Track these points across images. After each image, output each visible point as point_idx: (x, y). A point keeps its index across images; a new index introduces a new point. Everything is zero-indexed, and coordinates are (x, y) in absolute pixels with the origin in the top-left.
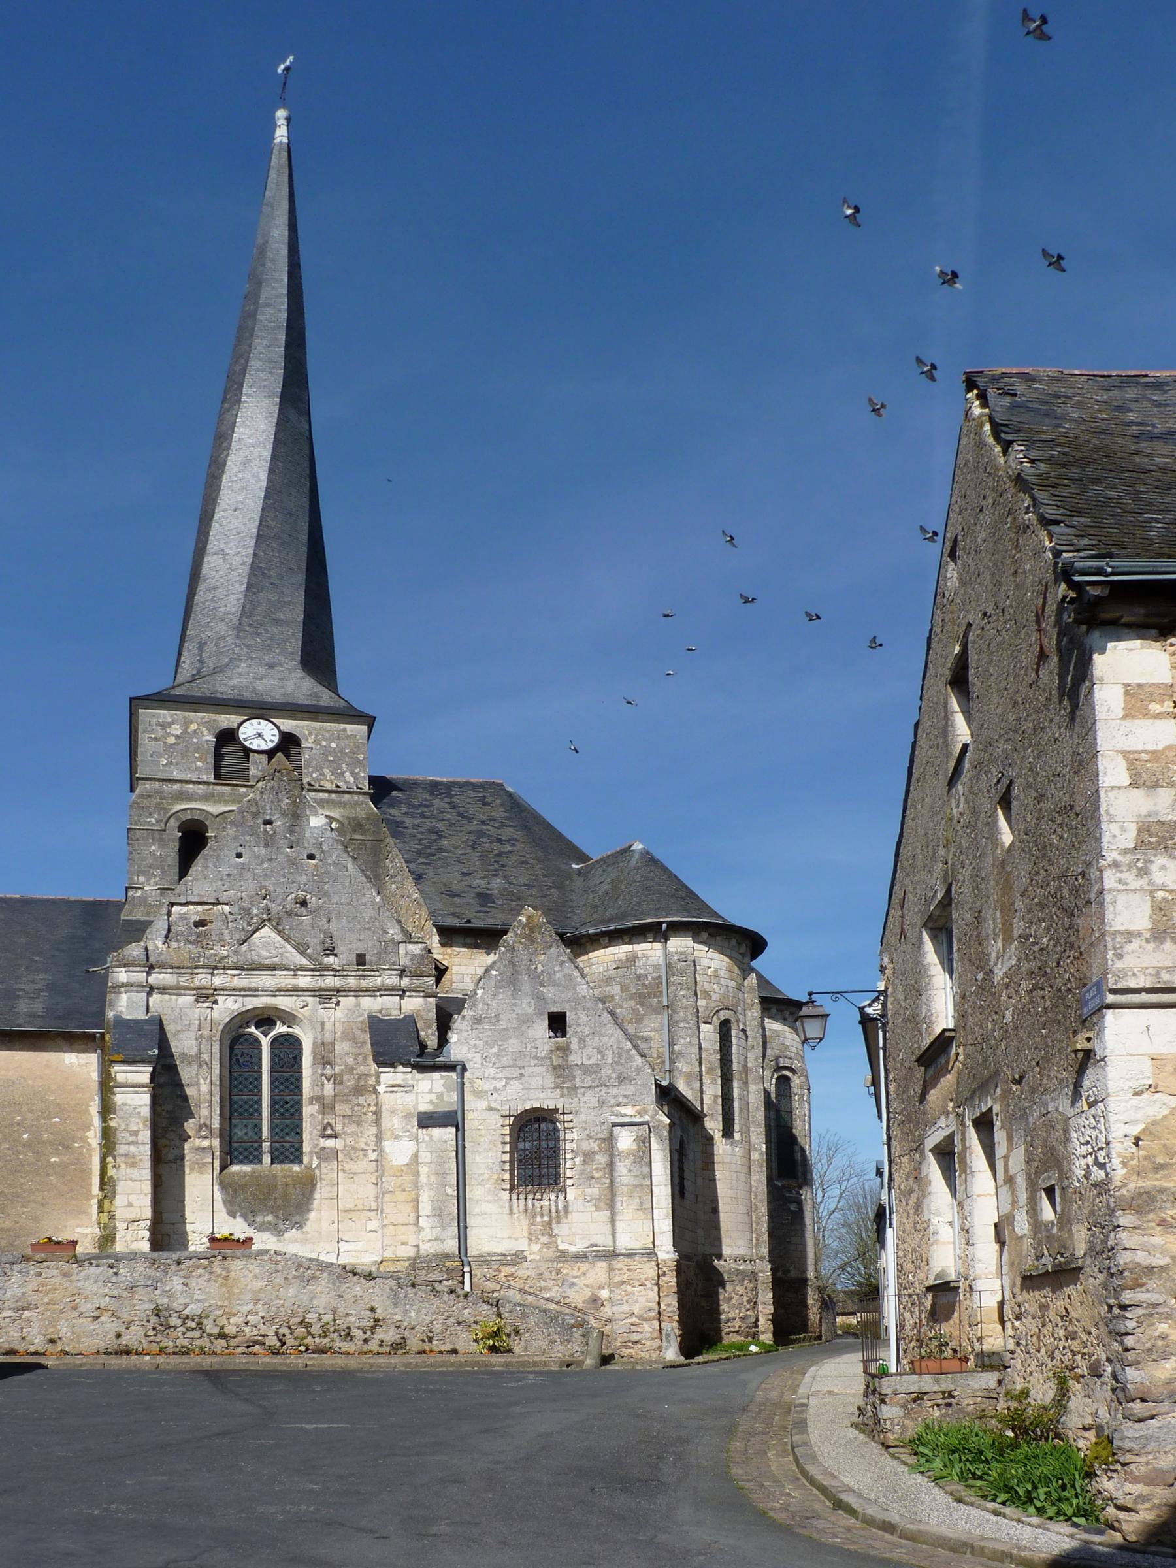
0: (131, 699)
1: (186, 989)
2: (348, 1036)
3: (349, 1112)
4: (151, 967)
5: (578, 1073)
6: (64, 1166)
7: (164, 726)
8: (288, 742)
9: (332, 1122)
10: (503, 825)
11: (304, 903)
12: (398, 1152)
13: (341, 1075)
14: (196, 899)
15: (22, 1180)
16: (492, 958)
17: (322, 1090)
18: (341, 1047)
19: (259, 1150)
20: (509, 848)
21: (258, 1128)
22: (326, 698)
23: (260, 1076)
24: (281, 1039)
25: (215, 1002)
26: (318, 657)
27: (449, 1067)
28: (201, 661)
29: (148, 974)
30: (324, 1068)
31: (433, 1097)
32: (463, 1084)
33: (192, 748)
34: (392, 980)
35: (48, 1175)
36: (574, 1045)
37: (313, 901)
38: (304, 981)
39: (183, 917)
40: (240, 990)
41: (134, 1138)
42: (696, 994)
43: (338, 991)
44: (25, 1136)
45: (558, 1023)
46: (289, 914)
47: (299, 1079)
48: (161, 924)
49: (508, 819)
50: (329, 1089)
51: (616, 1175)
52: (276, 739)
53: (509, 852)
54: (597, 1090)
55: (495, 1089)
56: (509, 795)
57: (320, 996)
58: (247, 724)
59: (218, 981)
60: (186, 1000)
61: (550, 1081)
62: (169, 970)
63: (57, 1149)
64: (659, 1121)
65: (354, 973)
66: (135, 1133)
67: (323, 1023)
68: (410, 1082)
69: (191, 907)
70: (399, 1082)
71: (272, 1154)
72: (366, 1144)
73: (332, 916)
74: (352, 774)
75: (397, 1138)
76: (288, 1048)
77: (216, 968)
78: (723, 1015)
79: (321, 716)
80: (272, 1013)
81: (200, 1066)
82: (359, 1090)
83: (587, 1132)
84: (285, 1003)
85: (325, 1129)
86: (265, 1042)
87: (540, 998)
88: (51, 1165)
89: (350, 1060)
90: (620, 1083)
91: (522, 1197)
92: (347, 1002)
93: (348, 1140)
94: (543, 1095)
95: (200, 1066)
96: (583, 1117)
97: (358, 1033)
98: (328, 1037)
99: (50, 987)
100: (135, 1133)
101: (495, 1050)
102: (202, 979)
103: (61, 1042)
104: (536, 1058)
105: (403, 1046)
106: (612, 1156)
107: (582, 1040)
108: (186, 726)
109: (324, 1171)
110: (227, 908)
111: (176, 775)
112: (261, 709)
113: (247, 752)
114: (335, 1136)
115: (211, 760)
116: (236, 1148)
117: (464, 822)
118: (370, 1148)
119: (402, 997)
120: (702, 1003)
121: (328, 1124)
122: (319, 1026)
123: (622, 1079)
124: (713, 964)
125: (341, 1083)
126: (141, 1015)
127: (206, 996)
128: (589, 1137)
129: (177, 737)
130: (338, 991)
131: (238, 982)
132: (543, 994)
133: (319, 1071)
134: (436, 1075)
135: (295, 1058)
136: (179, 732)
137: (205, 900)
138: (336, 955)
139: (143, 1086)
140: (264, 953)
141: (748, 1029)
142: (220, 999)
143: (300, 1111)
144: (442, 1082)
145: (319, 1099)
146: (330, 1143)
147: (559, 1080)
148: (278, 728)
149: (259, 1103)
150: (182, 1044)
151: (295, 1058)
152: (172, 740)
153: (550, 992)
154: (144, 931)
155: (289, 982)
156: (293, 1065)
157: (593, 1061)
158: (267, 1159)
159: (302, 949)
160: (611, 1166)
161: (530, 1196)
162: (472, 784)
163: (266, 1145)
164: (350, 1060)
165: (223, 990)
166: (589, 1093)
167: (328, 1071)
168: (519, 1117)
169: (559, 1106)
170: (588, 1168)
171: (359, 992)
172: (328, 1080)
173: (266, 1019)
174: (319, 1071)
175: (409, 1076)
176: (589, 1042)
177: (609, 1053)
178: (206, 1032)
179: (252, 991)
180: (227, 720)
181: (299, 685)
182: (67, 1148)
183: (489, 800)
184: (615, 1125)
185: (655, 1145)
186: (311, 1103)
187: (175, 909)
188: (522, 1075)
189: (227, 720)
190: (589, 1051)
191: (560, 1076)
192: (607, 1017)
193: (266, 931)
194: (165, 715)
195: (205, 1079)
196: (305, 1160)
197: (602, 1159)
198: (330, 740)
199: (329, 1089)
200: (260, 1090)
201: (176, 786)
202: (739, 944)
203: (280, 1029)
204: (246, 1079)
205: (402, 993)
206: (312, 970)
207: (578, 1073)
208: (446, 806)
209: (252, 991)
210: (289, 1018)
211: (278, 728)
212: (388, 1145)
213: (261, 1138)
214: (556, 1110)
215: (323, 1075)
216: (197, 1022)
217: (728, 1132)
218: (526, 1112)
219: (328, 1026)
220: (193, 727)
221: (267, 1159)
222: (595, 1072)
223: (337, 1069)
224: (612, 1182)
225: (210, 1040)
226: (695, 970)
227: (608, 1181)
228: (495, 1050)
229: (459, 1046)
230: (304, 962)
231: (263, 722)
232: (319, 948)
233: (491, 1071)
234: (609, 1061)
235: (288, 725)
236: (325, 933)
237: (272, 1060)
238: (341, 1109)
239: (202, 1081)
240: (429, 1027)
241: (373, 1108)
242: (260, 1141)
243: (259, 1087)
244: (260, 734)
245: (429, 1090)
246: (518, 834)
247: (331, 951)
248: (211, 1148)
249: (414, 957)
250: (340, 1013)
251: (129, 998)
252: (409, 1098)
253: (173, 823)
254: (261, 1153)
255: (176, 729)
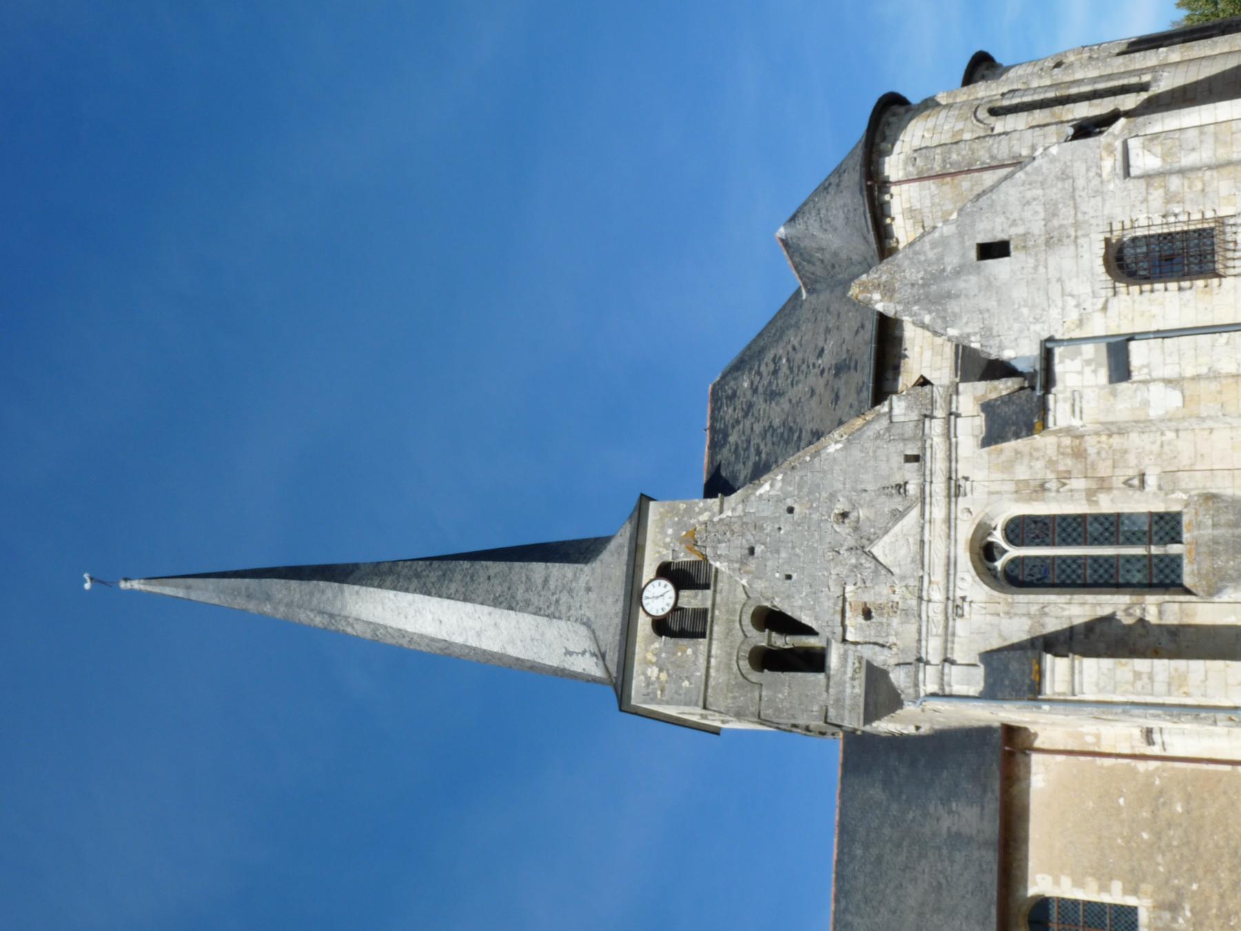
0: (642, 495)
1: (946, 627)
2: (1008, 466)
3: (1110, 463)
4: (919, 660)
5: (1056, 223)
6: (1188, 798)
7: (649, 683)
8: (665, 571)
9: (1122, 479)
10: (759, 373)
11: (844, 515)
12: (1163, 401)
13: (1058, 472)
14: (838, 618)
15: (1211, 846)
16: (906, 319)
17: (1077, 490)
18: (1022, 472)
19: (1161, 558)
20: (784, 361)
21: (1128, 559)
22: (622, 540)
23: (1060, 557)
24: (1012, 537)
25: (963, 599)
26: (579, 551)
27: (1047, 356)
28: (583, 653)
29: (927, 663)
30: (1049, 490)
31: (1088, 370)
32: (1071, 340)
33: (673, 659)
34: (936, 428)
35: (1202, 816)
36: (1020, 230)
37: (839, 508)
38: (938, 511)
39: (860, 629)
40: (948, 574)
41: (1145, 677)
42: (957, 143)
43: (950, 478)
44: (1145, 836)
45: (993, 250)
46: (856, 529)
47: (1064, 518)
48: (868, 652)
49: (751, 369)
50: (1078, 484)
51: (1198, 164)
52: (664, 582)
53: (788, 360)
54: (1079, 200)
55: (1077, 306)
56: (723, 377)
57: (957, 496)
58: (648, 608)
59: (937, 595)
60: (960, 626)
61: (1068, 251)
62: (924, 643)
63: (1164, 804)
64: (1123, 130)
65: (928, 464)
66: (1137, 675)
67: (990, 493)
68: (1068, 394)
69: (847, 622)
70: (1068, 407)
71: (1166, 544)
72: (1153, 443)
73: (860, 487)
74: (700, 513)
75: (1146, 403)
76: (1019, 530)
77: (920, 598)
78: (983, 114)
79: (640, 542)
80: (977, 545)
81: (1046, 614)
82: (1079, 454)
83: (1137, 203)
84: (965, 531)
85: (1131, 486)
86: (1014, 552)
87: (958, 272)
88: (1188, 812)
89: (1039, 465)
90: (1068, 177)
91: (1230, 263)
92: (963, 469)
93: (1146, 461)
94: (1086, 256)
95: (1046, 614)
96: (1118, 210)
97: (1003, 458)
98: (1010, 487)
99: (945, 801)
100: (1137, 675)
101: (1025, 311)
102: (935, 611)
103: (1015, 790)
104: (1036, 268)
105: (1020, 398)
106: (1171, 173)
107: (1014, 223)
108: (649, 664)
109: (1192, 485)
110: (849, 588)
111: (700, 673)
112: (634, 596)
113: (675, 608)
114: (1142, 477)
115: (683, 642)
116: (1165, 578)
117: (755, 410)
118: (1159, 439)
119: (958, 416)
120: (967, 136)
121: (1126, 483)
122: (993, 497)
123: (1064, 176)
124: (919, 134)
125: (1069, 472)
126: (980, 671)
127: (955, 608)
128: (1145, 200)
129: (661, 670)
130: (950, 478)
131: (939, 576)
132: (954, 269)
133: (1053, 494)
134: (1058, 368)
135: (1035, 522)
136: (656, 670)
137: (839, 608)
138: (906, 483)
139: (1073, 668)
140: (903, 552)
141: (1000, 92)
142: (959, 593)
143: (1106, 517)
144: (1067, 361)
145: (1090, 495)
146: (1151, 481)
147: (1066, 241)
148: (651, 581)
149: (1095, 559)
150: (1017, 630)
151: (1035, 522)
152: (663, 676)
153: (952, 261)
154: (877, 669)
155: (939, 528)
156: (1045, 524)
157: (1040, 209)
158: (1174, 549)
159: (897, 516)
160: (1182, 172)
161: (1230, 254)
162: (713, 411)
163: (1155, 550)
164: (1039, 465)
165: (948, 590)
166: (1083, 207)
167: (1053, 485)
168: (1116, 279)
169: (1102, 237)
170: (1189, 196)
171: (951, 458)
172: (1064, 484)
173: (985, 552)
174: (1053, 494)
175: (1060, 396)
176: (1016, 215)
177: (1029, 195)
178: (1001, 608)
179: (950, 564)
180: (644, 626)
181: (612, 562)
182: (1161, 792)
183: (730, 392)
184: (1127, 174)
185: (1157, 128)
186: (1096, 503)
187: (849, 637)
188: (1059, 280)
189: (644, 626)
190: (1028, 214)
191: (1060, 240)
192: (984, 201)
193: (877, 550)
194: (637, 683)
195: (1063, 609)
196: (1175, 508)
197: (1175, 183)
198: (666, 535)
199: (1078, 484)
200: (1079, 557)
201: (713, 672)
202: (894, 115)
203: (998, 537)
204: (1064, 571)
205: (952, 415)
206: (923, 503)
207: (1056, 223)
208: (737, 428)
209: (950, 564)
210: (983, 529)
211: (651, 581)
212: (1154, 413)
213: (1144, 556)
214: (1107, 241)
215: (1058, 491)
216: (989, 618)
217: (1143, 87)
218: (1109, 271)
219: (995, 487)
220: (650, 657)
221: (1174, 549)
222: (1056, 204)
223: (1051, 476)
224: (1210, 168)
225: (1011, 604)
226: (926, 148)
227: (1208, 173)
228: (1025, 311)
229: (1020, 350)
230: (915, 513)
231: (646, 594)
232: (898, 499)
233: (1054, 313)
234: (1040, 192)
235: (649, 570)
236: (880, 495)
237: (1038, 545)
238: (1103, 470)
239: (1066, 613)
240: (996, 388)
241: (1104, 438)
242: (1150, 557)
243: (1075, 559)
244: (659, 598)
245: (1079, 375)
246: (770, 355)
247: (901, 488)
248: (1160, 605)
249: (909, 408)
250: (978, 475)
251: (958, 683)
252: (1089, 395)
253: (755, 676)
254: (1167, 556)
255: (653, 672)
